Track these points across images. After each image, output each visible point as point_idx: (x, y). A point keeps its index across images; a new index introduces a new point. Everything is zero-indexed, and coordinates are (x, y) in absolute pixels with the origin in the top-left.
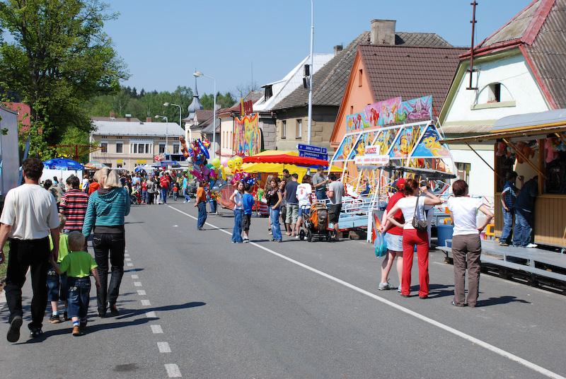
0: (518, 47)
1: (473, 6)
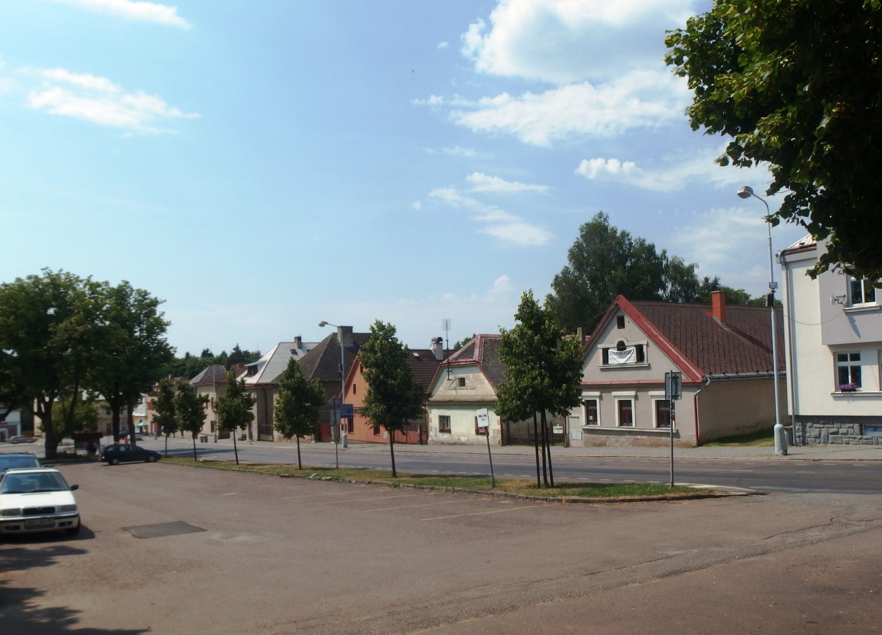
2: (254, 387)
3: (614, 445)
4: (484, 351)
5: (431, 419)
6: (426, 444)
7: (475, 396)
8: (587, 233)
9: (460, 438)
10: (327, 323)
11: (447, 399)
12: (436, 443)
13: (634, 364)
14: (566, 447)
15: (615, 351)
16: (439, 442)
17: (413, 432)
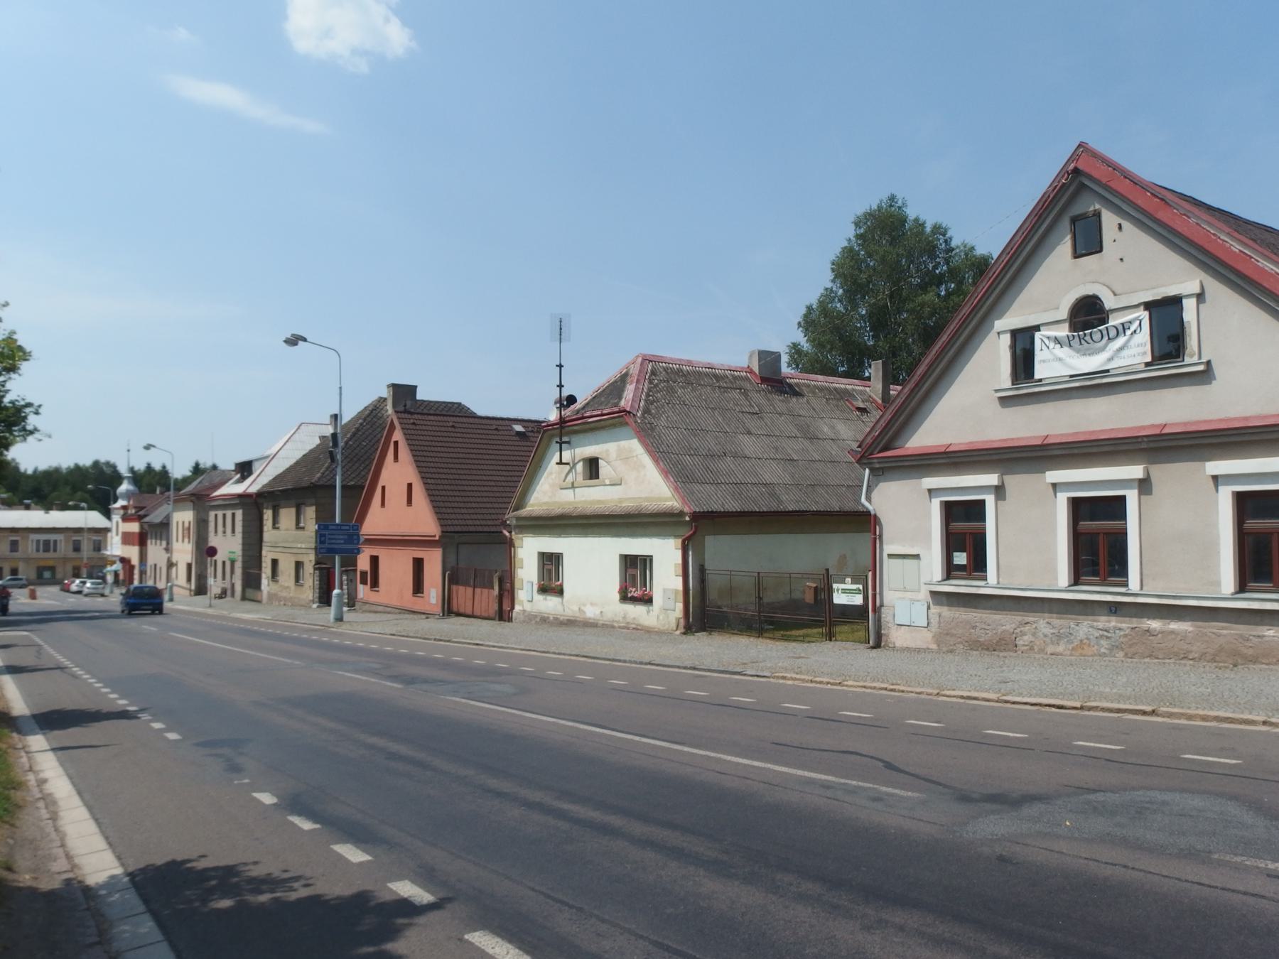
0: (622, 416)
1: (558, 368)
2: (237, 501)
3: (1050, 649)
4: (649, 390)
5: (522, 560)
6: (510, 620)
7: (621, 501)
8: (871, 230)
9: (583, 608)
10: (305, 340)
11: (558, 511)
13: (1142, 367)
14: (873, 648)
15: (1063, 331)
16: (536, 616)
17: (485, 591)
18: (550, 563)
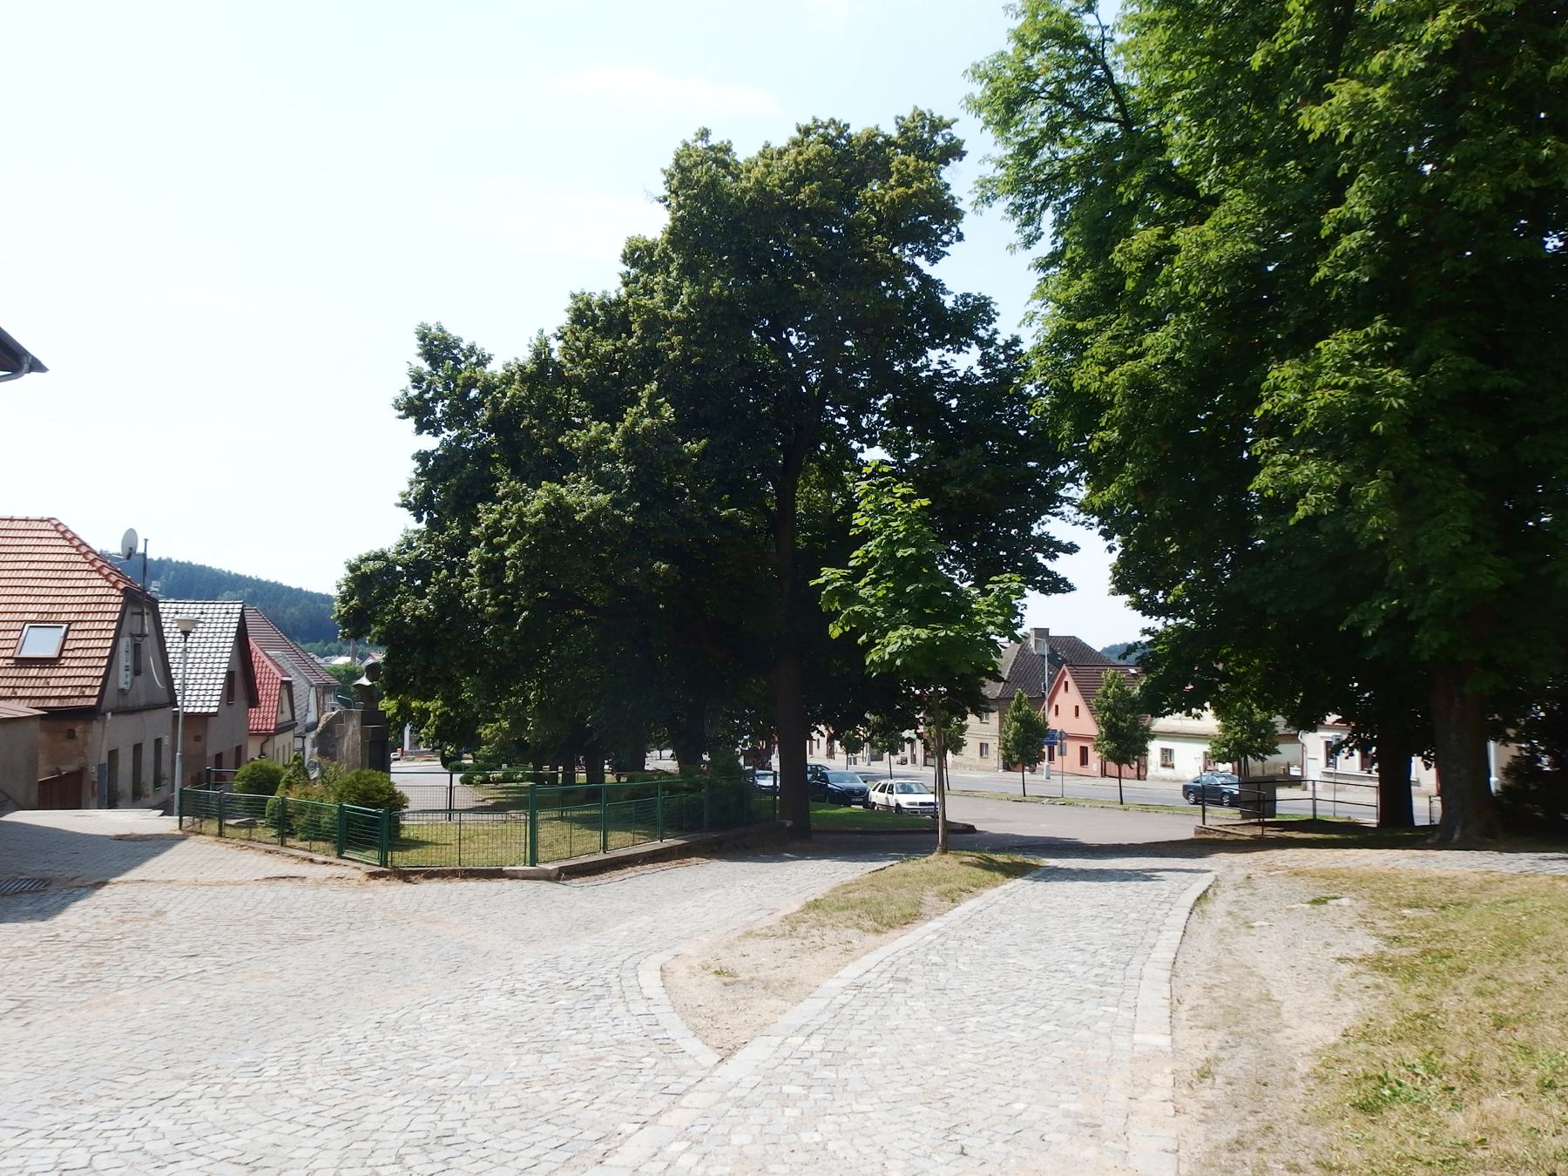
6: (1145, 779)
11: (1171, 730)
12: (1156, 779)
18: (1167, 754)
